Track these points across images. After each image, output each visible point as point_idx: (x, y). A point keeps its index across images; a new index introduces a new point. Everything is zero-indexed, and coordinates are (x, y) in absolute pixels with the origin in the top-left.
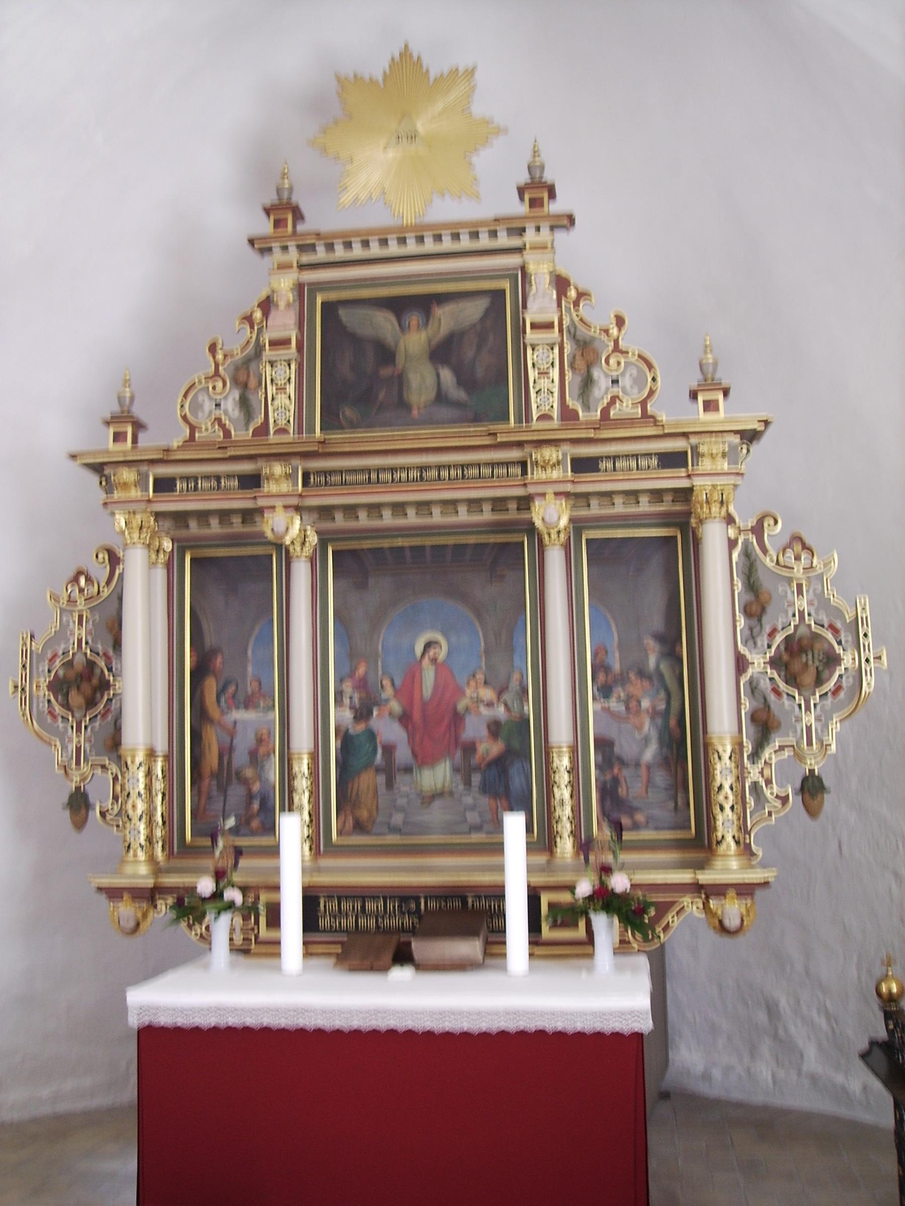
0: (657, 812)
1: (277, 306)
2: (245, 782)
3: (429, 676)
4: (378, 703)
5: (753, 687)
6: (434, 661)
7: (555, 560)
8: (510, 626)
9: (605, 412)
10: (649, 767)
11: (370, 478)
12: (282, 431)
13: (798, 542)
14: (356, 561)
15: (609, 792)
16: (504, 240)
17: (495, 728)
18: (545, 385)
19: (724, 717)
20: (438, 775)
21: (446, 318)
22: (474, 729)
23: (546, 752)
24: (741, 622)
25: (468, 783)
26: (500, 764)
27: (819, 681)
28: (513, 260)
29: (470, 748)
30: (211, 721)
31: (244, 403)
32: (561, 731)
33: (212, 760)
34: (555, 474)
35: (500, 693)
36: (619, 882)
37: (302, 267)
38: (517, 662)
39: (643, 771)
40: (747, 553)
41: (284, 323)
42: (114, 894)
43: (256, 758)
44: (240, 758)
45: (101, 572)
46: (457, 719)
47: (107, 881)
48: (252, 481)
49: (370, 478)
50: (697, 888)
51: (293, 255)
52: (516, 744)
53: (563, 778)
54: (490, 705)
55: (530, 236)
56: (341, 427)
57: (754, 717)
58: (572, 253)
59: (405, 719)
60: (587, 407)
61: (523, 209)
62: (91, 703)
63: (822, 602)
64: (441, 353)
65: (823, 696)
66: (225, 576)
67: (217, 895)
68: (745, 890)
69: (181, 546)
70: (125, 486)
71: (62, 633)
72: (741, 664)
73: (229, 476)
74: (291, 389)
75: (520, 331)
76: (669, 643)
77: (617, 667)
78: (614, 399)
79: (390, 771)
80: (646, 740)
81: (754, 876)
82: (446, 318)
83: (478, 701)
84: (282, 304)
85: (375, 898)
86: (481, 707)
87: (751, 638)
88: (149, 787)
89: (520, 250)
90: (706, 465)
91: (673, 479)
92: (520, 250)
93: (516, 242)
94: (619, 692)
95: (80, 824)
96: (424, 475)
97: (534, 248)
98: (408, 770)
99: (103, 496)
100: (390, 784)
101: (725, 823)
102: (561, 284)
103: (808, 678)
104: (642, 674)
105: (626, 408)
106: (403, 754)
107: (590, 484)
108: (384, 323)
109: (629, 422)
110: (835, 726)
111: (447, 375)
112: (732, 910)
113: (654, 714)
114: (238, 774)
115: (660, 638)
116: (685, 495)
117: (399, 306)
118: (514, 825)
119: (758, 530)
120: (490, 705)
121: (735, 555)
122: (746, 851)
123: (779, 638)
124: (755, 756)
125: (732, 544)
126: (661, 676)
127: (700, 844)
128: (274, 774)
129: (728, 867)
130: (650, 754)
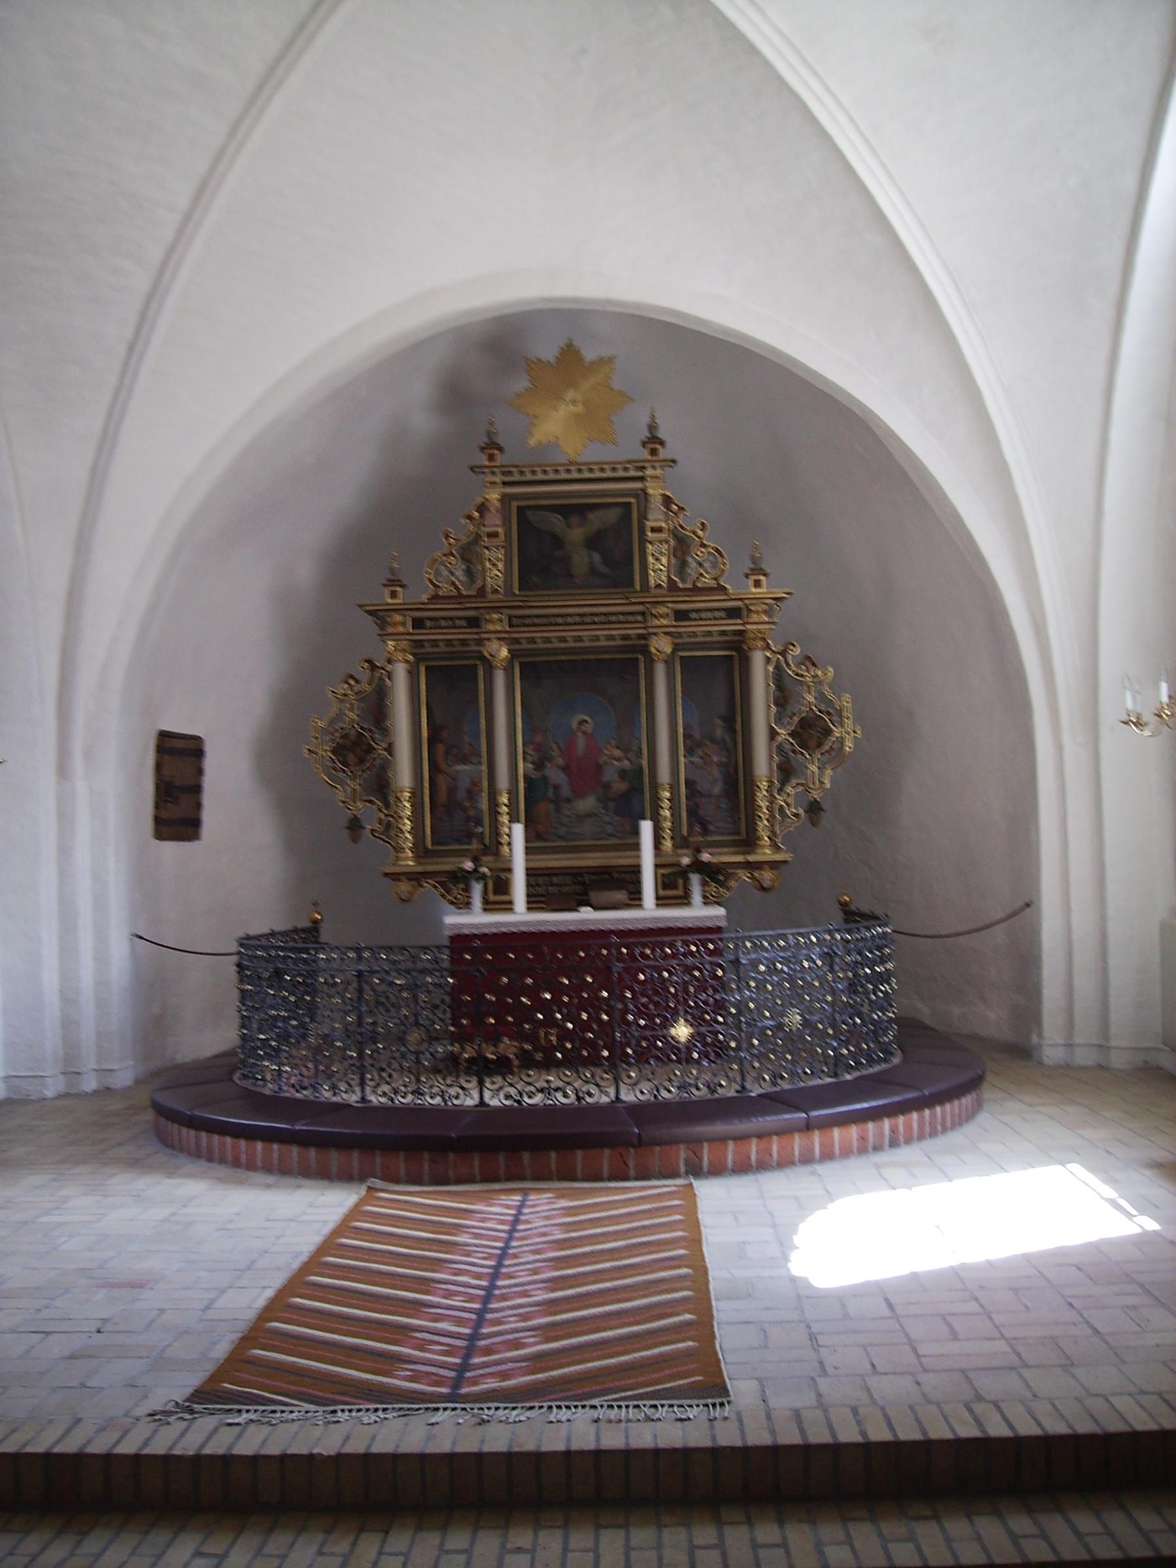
0: (721, 824)
2: (464, 809)
3: (581, 742)
4: (550, 759)
5: (780, 749)
6: (584, 733)
7: (660, 671)
8: (630, 710)
11: (549, 622)
13: (809, 660)
14: (534, 669)
15: (692, 812)
16: (633, 473)
17: (623, 774)
18: (659, 566)
19: (763, 764)
20: (588, 804)
21: (596, 520)
22: (610, 775)
23: (655, 787)
24: (774, 708)
25: (606, 808)
26: (626, 796)
28: (638, 485)
29: (607, 787)
30: (441, 771)
31: (469, 573)
32: (664, 776)
33: (443, 796)
34: (664, 622)
36: (705, 857)
37: (504, 483)
40: (778, 667)
41: (494, 522)
42: (395, 877)
43: (472, 794)
44: (461, 795)
45: (364, 675)
46: (599, 768)
47: (390, 869)
48: (474, 622)
49: (549, 622)
50: (748, 865)
51: (498, 479)
53: (666, 804)
55: (649, 472)
56: (530, 589)
57: (781, 767)
59: (566, 769)
60: (683, 581)
61: (645, 454)
62: (361, 761)
63: (821, 697)
64: (593, 542)
66: (452, 681)
67: (475, 870)
68: (774, 865)
69: (419, 658)
70: (395, 624)
71: (340, 716)
72: (773, 734)
73: (460, 618)
74: (501, 566)
75: (642, 532)
76: (729, 721)
79: (558, 801)
80: (715, 781)
81: (779, 857)
82: (596, 520)
84: (492, 509)
86: (614, 761)
87: (779, 719)
89: (642, 479)
90: (755, 618)
91: (732, 626)
92: (642, 479)
93: (640, 474)
95: (355, 839)
96: (583, 620)
97: (652, 477)
98: (569, 800)
99: (376, 630)
100: (558, 810)
101: (763, 826)
102: (667, 501)
103: (812, 744)
104: (713, 740)
105: (707, 581)
106: (566, 791)
107: (686, 628)
108: (556, 522)
110: (829, 772)
111: (597, 557)
112: (767, 876)
113: (720, 765)
115: (724, 719)
116: (740, 633)
117: (565, 511)
118: (646, 827)
119: (783, 653)
121: (771, 669)
122: (775, 847)
123: (796, 719)
124: (780, 791)
125: (768, 660)
126: (723, 739)
127: (749, 842)
128: (484, 805)
129: (766, 853)
130: (717, 789)
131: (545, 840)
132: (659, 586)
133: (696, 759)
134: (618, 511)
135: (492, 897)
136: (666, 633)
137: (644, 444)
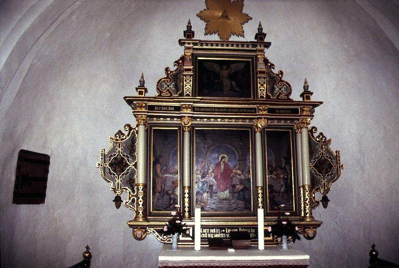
1: (187, 60)
6: (224, 162)
7: (258, 135)
9: (278, 96)
10: (283, 193)
12: (188, 95)
18: (262, 90)
27: (327, 172)
30: (158, 177)
31: (176, 86)
35: (242, 172)
38: (247, 164)
39: (281, 194)
52: (247, 186)
54: (239, 175)
55: (258, 48)
58: (269, 53)
61: (136, 94)
64: (232, 77)
65: (328, 176)
71: (114, 150)
77: (274, 166)
78: (280, 93)
83: (236, 174)
85: (213, 228)
88: (305, 207)
94: (275, 173)
95: (118, 206)
104: (281, 168)
108: (217, 68)
109: (284, 100)
111: (234, 83)
114: (167, 192)
120: (239, 175)
131: (205, 211)
132: (262, 97)
133: (273, 176)
134: (244, 64)
135: (253, 231)
136: (265, 118)
137: (137, 89)
